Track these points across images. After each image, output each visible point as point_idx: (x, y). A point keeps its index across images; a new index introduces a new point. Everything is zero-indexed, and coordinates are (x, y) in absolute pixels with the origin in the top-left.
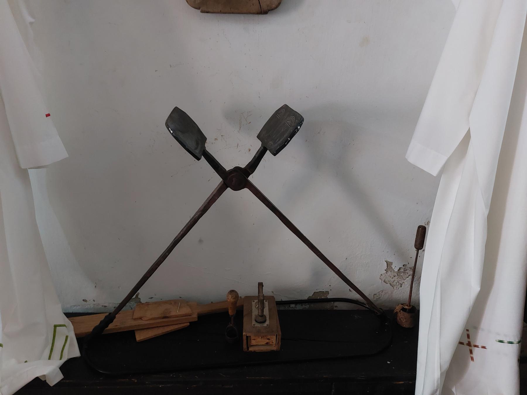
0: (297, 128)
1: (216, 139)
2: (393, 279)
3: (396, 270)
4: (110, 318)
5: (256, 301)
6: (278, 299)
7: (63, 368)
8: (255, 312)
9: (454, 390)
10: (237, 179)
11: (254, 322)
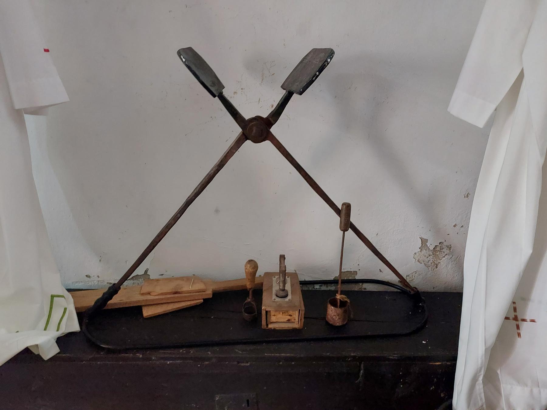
0: (326, 61)
1: (235, 93)
2: (428, 259)
3: (432, 248)
4: (114, 289)
5: (277, 277)
6: (302, 278)
7: (60, 341)
8: (276, 287)
9: (499, 372)
10: (258, 130)
11: (274, 297)
